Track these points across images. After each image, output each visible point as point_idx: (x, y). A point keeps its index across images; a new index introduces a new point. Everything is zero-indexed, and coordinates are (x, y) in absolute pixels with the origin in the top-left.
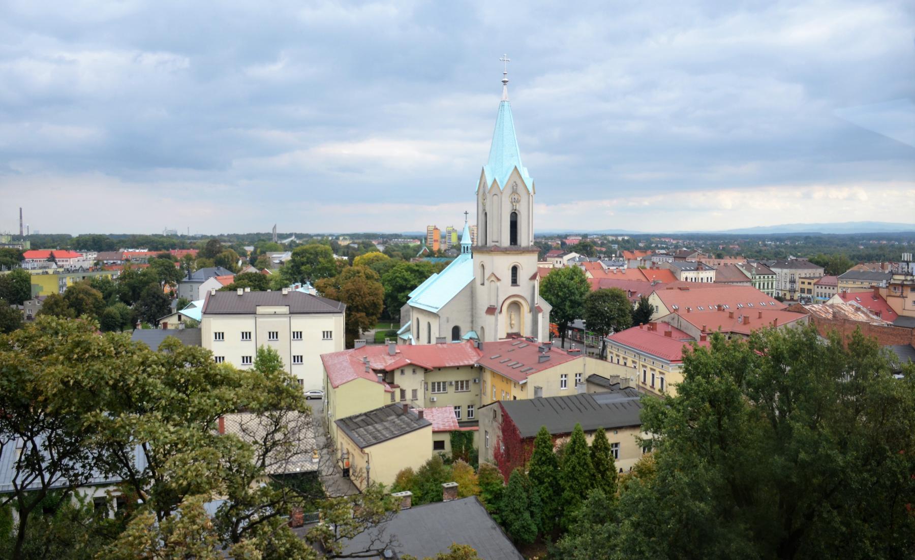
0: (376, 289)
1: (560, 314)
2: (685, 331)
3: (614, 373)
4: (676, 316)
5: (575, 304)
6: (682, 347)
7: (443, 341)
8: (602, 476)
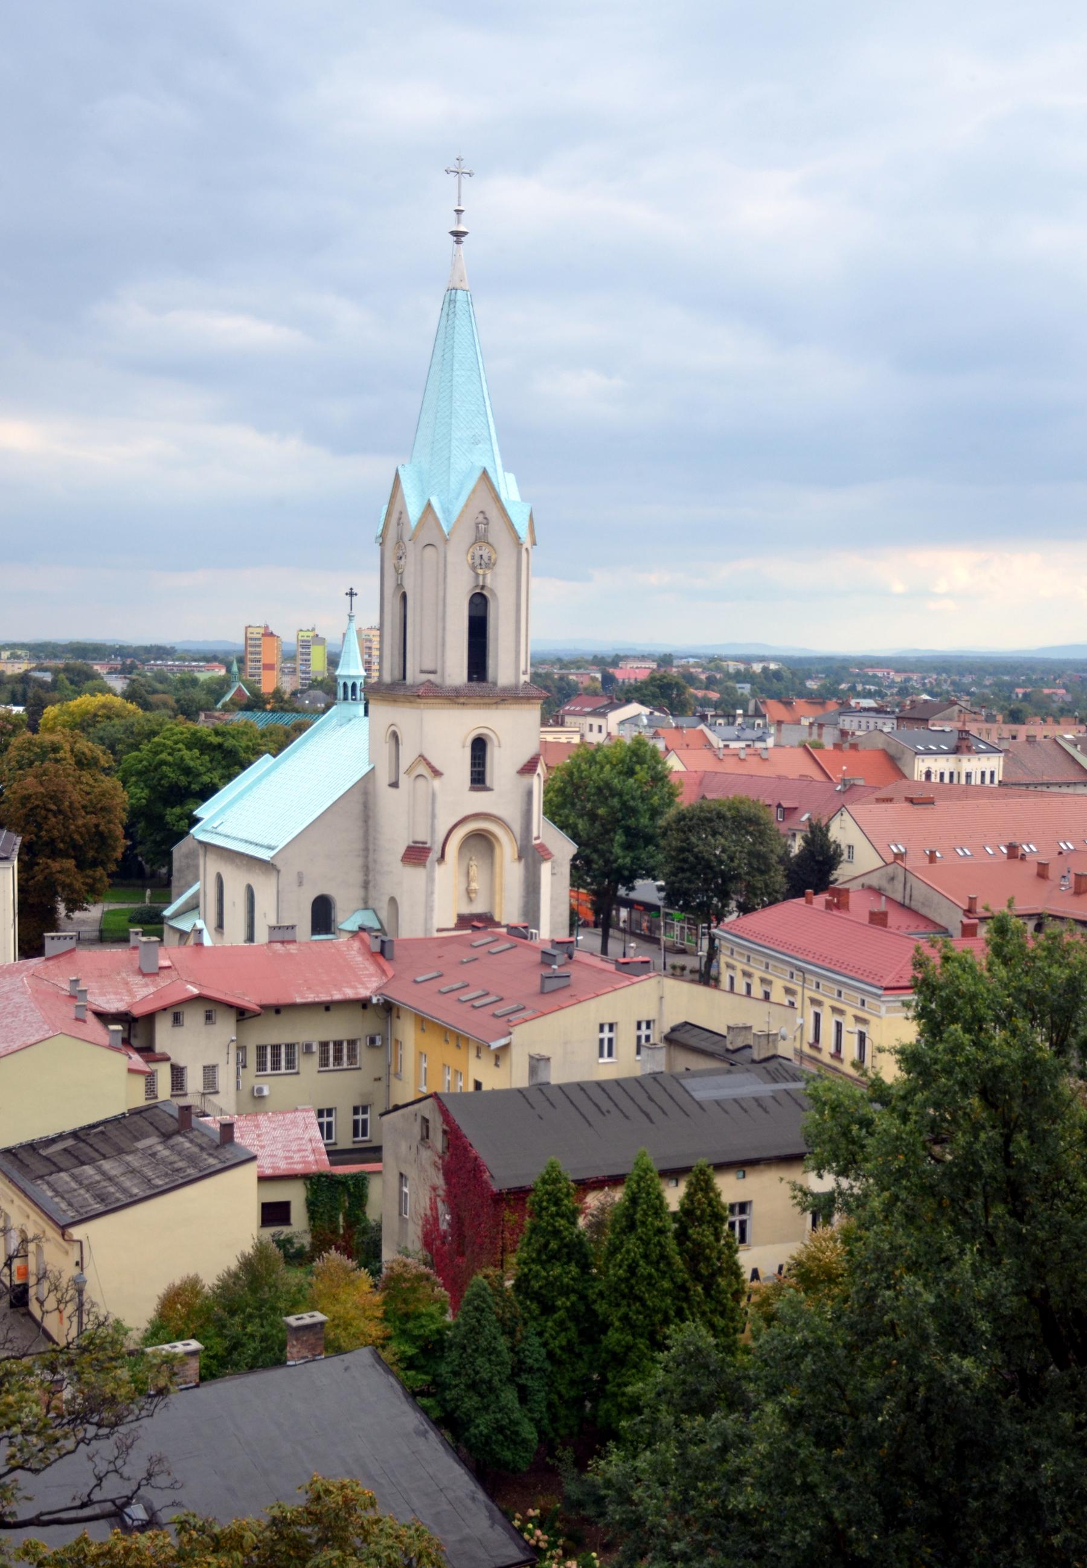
0: (103, 794)
1: (598, 863)
2: (924, 911)
4: (900, 872)
5: (637, 838)
8: (707, 1289)
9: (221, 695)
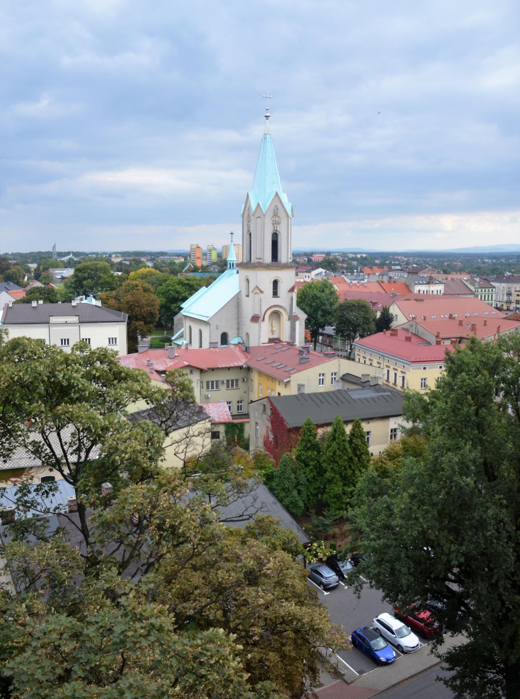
0: (152, 300)
1: (313, 321)
2: (422, 336)
3: (366, 373)
4: (414, 323)
5: (326, 313)
6: (445, 350)
7: (215, 345)
8: (359, 459)
9: (183, 268)
